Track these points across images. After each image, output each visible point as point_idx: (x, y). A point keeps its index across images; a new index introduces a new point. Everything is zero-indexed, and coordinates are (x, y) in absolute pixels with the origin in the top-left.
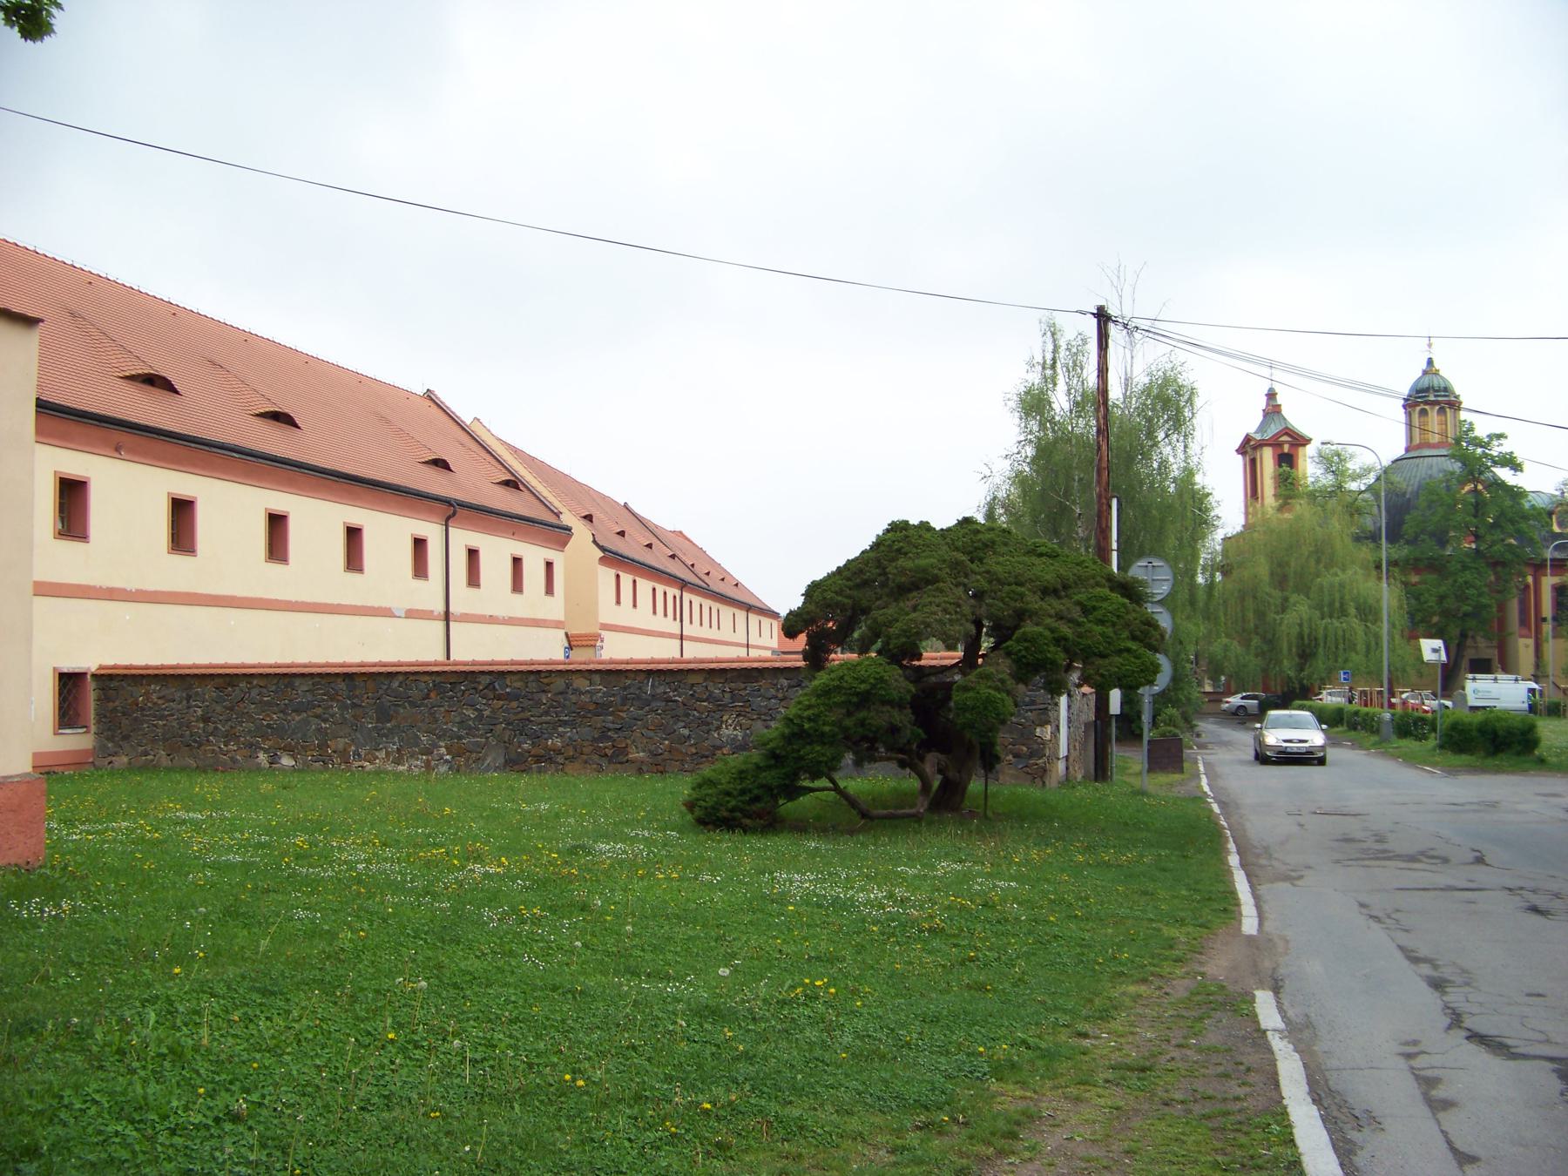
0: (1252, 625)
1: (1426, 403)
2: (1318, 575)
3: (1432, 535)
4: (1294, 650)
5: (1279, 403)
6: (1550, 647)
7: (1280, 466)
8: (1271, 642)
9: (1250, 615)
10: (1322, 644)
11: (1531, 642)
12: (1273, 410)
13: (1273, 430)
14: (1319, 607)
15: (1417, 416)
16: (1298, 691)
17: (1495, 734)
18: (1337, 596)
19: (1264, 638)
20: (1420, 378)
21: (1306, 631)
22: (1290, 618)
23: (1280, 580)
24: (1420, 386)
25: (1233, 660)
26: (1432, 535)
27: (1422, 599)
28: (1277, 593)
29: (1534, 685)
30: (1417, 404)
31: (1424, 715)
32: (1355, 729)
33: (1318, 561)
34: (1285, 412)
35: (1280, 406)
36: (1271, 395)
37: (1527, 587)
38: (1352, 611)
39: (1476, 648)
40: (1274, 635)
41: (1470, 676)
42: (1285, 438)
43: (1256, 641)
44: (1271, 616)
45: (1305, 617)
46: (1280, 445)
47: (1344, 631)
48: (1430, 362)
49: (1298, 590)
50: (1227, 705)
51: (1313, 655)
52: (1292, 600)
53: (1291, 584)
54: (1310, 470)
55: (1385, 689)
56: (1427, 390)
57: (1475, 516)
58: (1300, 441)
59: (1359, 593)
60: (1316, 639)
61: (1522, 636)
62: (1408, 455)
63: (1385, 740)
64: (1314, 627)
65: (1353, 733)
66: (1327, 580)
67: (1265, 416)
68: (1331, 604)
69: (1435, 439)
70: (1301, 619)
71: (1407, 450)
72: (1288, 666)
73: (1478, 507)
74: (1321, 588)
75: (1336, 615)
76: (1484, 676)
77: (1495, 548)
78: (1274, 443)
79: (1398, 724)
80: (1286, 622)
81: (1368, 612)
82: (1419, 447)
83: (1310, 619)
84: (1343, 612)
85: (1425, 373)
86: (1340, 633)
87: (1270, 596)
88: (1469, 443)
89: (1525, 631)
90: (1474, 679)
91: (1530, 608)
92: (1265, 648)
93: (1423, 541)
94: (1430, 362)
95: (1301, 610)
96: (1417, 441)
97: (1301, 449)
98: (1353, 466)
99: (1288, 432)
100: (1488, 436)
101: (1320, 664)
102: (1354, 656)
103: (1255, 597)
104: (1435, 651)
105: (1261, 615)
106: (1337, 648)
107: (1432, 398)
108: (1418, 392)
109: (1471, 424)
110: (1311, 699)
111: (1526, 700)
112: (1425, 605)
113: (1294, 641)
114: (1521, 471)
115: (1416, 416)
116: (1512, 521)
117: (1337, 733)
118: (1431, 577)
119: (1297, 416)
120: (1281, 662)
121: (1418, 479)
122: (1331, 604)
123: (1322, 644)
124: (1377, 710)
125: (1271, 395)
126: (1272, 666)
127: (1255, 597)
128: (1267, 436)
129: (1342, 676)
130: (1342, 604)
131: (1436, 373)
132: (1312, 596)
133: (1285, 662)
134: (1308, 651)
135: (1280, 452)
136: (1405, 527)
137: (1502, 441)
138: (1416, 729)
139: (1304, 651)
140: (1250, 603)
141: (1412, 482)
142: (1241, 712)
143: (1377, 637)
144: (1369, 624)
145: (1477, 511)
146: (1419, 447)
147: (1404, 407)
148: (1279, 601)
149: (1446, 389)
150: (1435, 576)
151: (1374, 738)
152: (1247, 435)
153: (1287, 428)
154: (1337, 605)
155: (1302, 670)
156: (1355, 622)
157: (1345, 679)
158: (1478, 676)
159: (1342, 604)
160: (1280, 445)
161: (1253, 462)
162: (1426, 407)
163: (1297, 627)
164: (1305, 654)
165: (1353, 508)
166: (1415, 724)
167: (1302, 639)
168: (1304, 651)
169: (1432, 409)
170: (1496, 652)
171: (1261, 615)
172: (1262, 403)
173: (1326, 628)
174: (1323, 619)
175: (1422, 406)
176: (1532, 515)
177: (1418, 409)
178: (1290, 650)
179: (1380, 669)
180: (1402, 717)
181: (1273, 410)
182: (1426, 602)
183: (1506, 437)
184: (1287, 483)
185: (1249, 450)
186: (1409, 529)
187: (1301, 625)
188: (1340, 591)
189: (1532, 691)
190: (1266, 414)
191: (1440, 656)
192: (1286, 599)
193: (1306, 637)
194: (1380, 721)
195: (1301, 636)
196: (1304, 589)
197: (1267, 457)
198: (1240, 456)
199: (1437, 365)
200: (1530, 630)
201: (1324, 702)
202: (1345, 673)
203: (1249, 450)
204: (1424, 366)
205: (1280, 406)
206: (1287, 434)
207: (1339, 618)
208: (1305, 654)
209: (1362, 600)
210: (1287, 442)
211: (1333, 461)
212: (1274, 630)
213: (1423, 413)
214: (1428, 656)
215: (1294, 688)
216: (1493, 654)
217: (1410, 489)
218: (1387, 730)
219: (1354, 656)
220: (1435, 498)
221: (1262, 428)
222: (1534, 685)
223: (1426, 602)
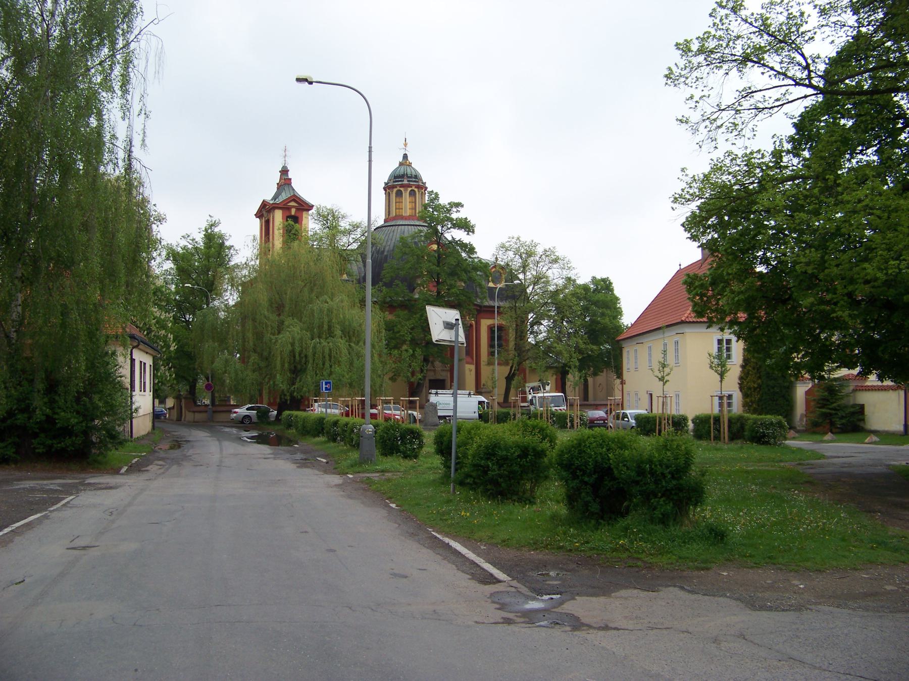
0: (251, 343)
1: (402, 186)
2: (311, 302)
3: (403, 280)
4: (286, 365)
5: (290, 177)
6: (485, 370)
7: (287, 221)
8: (267, 359)
9: (250, 335)
10: (311, 361)
11: (473, 367)
12: (285, 181)
13: (284, 196)
14: (310, 329)
15: (394, 195)
16: (289, 402)
17: (604, 471)
18: (326, 319)
19: (261, 356)
20: (398, 168)
21: (298, 349)
22: (285, 337)
23: (279, 308)
24: (397, 173)
25: (233, 375)
26: (403, 280)
27: (396, 329)
28: (274, 317)
29: (482, 399)
30: (393, 187)
31: (412, 426)
32: (334, 440)
33: (312, 290)
34: (294, 184)
35: (290, 179)
36: (284, 172)
37: (471, 325)
38: (338, 333)
39: (434, 371)
40: (270, 353)
41: (434, 391)
42: (293, 204)
43: (254, 358)
44: (267, 336)
45: (297, 337)
46: (289, 209)
47: (330, 350)
48: (405, 157)
49: (293, 315)
50: (235, 415)
51: (304, 370)
52: (286, 323)
53: (287, 309)
54: (312, 225)
55: (367, 399)
56: (402, 176)
57: (438, 266)
58: (305, 207)
59: (344, 318)
60: (306, 356)
61: (468, 363)
62: (386, 224)
63: (364, 461)
64: (304, 345)
65: (332, 444)
66: (317, 305)
67: (278, 189)
68: (321, 327)
69: (407, 212)
70: (293, 338)
71: (386, 221)
72: (281, 381)
73: (440, 259)
74: (313, 311)
75: (324, 336)
76: (444, 391)
77: (453, 290)
78: (284, 207)
79: (382, 437)
80: (280, 341)
81: (352, 334)
82: (395, 218)
83: (301, 339)
84: (330, 333)
85: (401, 164)
86: (327, 351)
87: (268, 319)
88: (434, 209)
89: (469, 360)
90: (437, 394)
91: (473, 341)
92: (263, 364)
93: (397, 285)
94: (405, 157)
95: (294, 330)
96: (393, 214)
97: (304, 213)
98: (344, 224)
99: (296, 198)
100: (449, 204)
101: (309, 378)
102: (337, 369)
103: (254, 320)
104: (449, 326)
105: (259, 336)
106: (324, 364)
107: (406, 182)
108: (395, 177)
109: (437, 194)
110: (305, 410)
111: (476, 410)
112: (398, 335)
113: (287, 360)
114: (473, 232)
115: (393, 196)
116: (466, 271)
117: (317, 444)
118: (403, 313)
119: (303, 188)
120: (275, 376)
121: (393, 241)
122: (321, 327)
123: (311, 361)
124: (358, 420)
125: (284, 172)
126: (266, 380)
127: (254, 320)
128: (280, 200)
129: (324, 386)
130: (330, 327)
131: (410, 165)
132: (304, 319)
133: (278, 376)
134: (299, 367)
135: (288, 214)
136: (383, 272)
137: (460, 209)
138: (404, 443)
139: (295, 367)
140: (249, 324)
141: (389, 243)
142: (247, 421)
143: (360, 356)
144: (352, 344)
145: (439, 263)
146: (395, 218)
147: (385, 189)
148: (275, 325)
149: (416, 177)
150: (406, 312)
151: (355, 455)
152: (264, 201)
153: (294, 195)
154: (326, 327)
155: (293, 384)
156: (342, 343)
157: (326, 389)
158: (440, 391)
159: (330, 327)
160: (289, 209)
161: (267, 222)
162: (401, 189)
163: (289, 345)
164: (296, 370)
165: (344, 256)
166: (403, 437)
167: (294, 357)
168: (295, 367)
169: (406, 190)
170: (449, 373)
171: (259, 336)
172: (277, 178)
173: (314, 347)
174: (312, 339)
175: (398, 188)
176: (480, 267)
177: (395, 190)
178: (283, 365)
179: (362, 378)
180: (387, 429)
181: (285, 181)
182: (399, 332)
183: (462, 206)
184: (293, 232)
185: (264, 213)
186: (387, 274)
187: (293, 344)
188: (328, 315)
189: (480, 403)
190: (279, 186)
191: (457, 335)
192: (282, 323)
193: (297, 356)
194: (360, 435)
195: (293, 353)
196: (296, 313)
197: (278, 216)
198: (258, 219)
199: (410, 159)
200: (472, 359)
201: (316, 412)
202: (326, 384)
203: (264, 213)
204: (401, 159)
205: (290, 179)
206: (294, 200)
207: (326, 338)
208: (296, 370)
209: (347, 323)
210: (293, 207)
211: (330, 219)
212: (270, 348)
213: (399, 194)
214: (438, 333)
215: (286, 400)
216: (443, 375)
217: (387, 248)
218: (369, 446)
219: (337, 369)
220: (407, 250)
221: (275, 198)
222: (482, 399)
223: (399, 332)
